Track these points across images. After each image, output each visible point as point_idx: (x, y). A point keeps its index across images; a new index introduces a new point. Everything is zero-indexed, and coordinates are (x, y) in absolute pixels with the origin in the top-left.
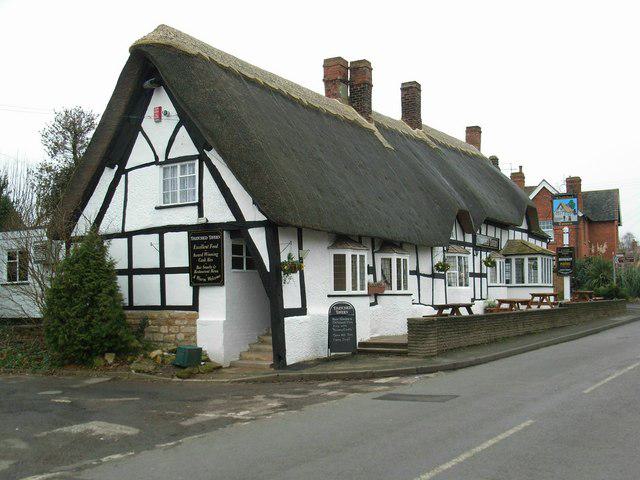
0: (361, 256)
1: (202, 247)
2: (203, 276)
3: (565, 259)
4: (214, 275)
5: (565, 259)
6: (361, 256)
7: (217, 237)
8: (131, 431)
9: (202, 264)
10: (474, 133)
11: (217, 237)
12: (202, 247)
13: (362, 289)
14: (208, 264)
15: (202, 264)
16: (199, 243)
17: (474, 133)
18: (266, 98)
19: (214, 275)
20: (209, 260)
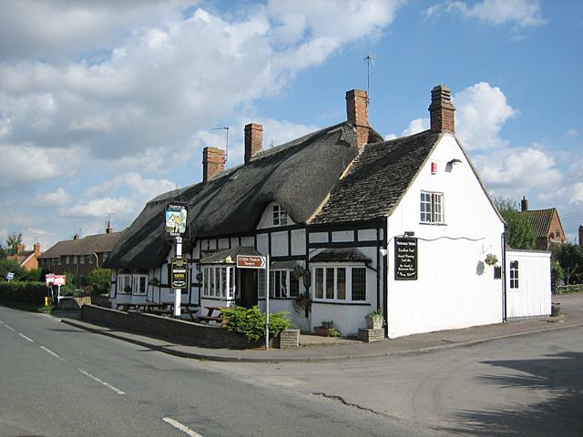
0: (328, 269)
1: (404, 250)
2: (404, 272)
3: (179, 271)
4: (412, 272)
5: (179, 271)
6: (328, 269)
7: (414, 244)
8: (341, 178)
9: (403, 263)
10: (524, 203)
11: (414, 244)
12: (404, 250)
13: (320, 271)
14: (408, 263)
15: (403, 263)
16: (402, 247)
17: (524, 203)
18: (56, 427)
19: (412, 272)
20: (409, 260)
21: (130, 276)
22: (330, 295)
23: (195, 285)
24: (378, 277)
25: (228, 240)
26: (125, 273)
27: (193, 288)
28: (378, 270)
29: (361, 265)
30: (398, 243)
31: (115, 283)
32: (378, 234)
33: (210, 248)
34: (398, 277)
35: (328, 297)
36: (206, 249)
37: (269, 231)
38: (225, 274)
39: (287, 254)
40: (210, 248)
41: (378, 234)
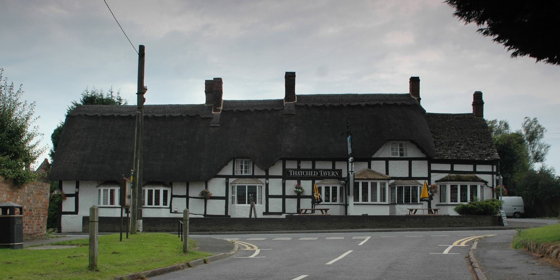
32: (493, 168)
35: (104, 203)
37: (387, 160)
41: (493, 168)
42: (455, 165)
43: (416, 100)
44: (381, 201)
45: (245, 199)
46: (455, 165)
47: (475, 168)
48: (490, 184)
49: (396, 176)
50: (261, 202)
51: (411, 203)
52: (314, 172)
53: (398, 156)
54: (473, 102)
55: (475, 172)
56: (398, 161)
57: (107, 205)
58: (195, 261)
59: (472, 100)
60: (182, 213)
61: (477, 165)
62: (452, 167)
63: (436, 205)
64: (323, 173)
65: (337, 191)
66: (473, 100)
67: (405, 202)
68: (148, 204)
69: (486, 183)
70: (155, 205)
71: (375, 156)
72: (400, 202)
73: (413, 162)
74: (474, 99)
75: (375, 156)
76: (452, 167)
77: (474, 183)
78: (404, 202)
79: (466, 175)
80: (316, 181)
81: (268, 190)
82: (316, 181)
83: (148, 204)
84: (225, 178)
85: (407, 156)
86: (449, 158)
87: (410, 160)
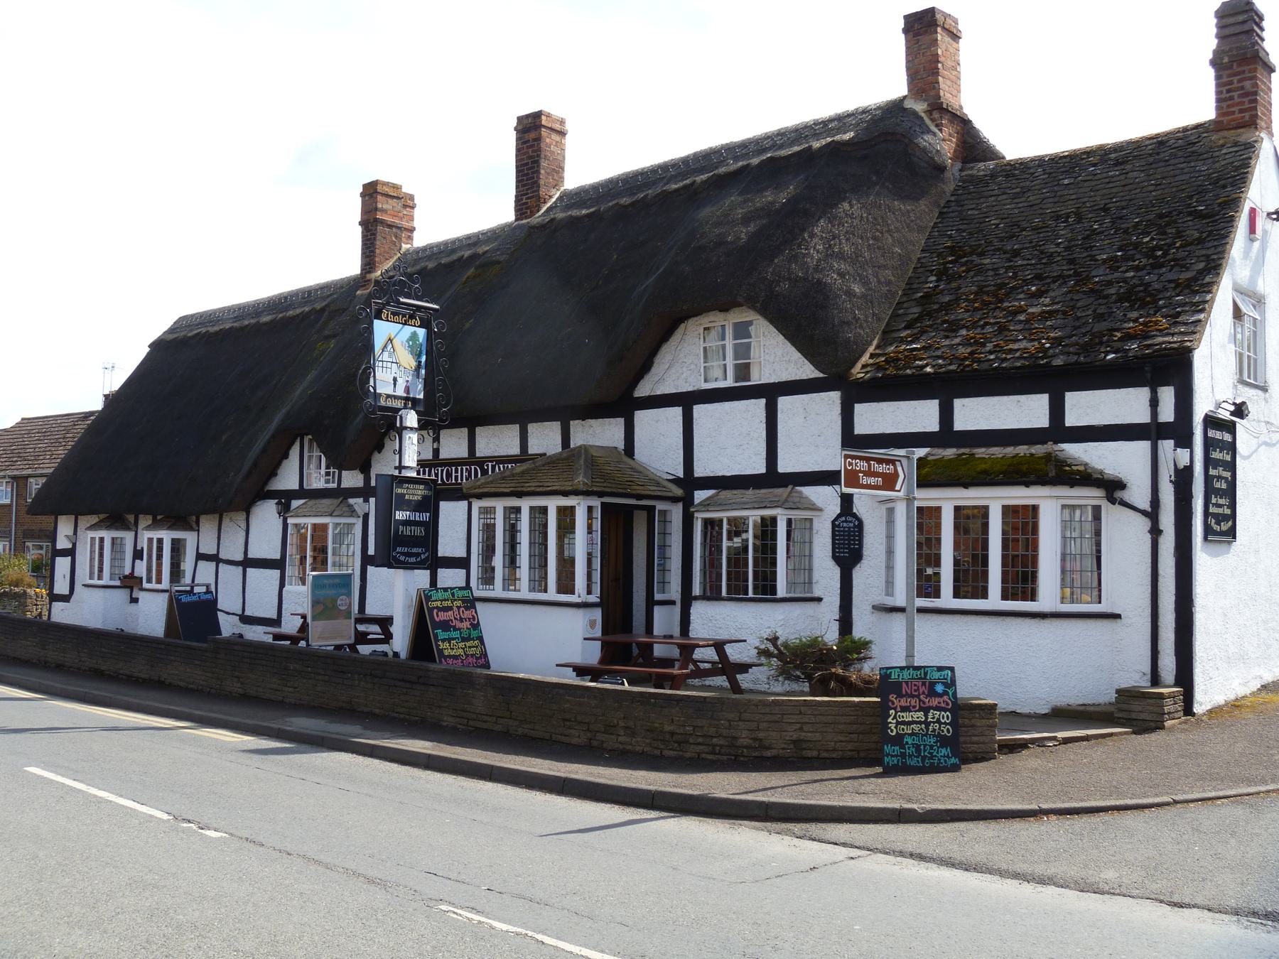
0: (1009, 511)
6: (1009, 511)
21: (128, 536)
22: (539, 582)
23: (64, 553)
24: (1156, 532)
25: (465, 431)
26: (109, 528)
27: (462, 553)
28: (1153, 514)
29: (1089, 496)
30: (1228, 437)
31: (71, 553)
32: (1154, 403)
33: (443, 455)
34: (749, 380)
35: (561, 590)
36: (463, 452)
37: (687, 401)
38: (512, 531)
39: (759, 467)
40: (444, 454)
41: (1154, 403)
42: (958, 403)
43: (923, 115)
44: (532, 589)
45: (729, 579)
46: (958, 403)
47: (1057, 410)
48: (1139, 494)
49: (720, 474)
50: (1100, 597)
51: (751, 595)
52: (471, 469)
53: (730, 382)
54: (1215, 52)
55: (1058, 430)
56: (727, 406)
57: (546, 591)
58: (1264, 922)
59: (1208, 42)
60: (233, 614)
61: (955, 400)
62: (946, 415)
63: (874, 607)
64: (493, 467)
65: (775, 539)
66: (1214, 43)
67: (728, 593)
68: (559, 591)
69: (1113, 488)
70: (1005, 597)
71: (643, 390)
72: (712, 594)
73: (784, 402)
74: (1221, 37)
75: (643, 390)
76: (946, 415)
77: (1019, 495)
78: (781, 591)
79: (1010, 451)
80: (696, 493)
81: (368, 536)
82: (696, 493)
83: (559, 591)
84: (362, 499)
85: (760, 380)
86: (928, 369)
87: (771, 393)
